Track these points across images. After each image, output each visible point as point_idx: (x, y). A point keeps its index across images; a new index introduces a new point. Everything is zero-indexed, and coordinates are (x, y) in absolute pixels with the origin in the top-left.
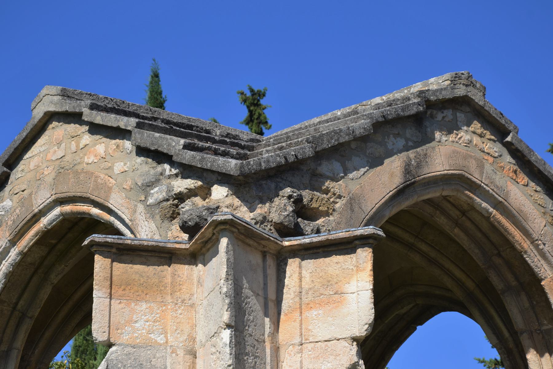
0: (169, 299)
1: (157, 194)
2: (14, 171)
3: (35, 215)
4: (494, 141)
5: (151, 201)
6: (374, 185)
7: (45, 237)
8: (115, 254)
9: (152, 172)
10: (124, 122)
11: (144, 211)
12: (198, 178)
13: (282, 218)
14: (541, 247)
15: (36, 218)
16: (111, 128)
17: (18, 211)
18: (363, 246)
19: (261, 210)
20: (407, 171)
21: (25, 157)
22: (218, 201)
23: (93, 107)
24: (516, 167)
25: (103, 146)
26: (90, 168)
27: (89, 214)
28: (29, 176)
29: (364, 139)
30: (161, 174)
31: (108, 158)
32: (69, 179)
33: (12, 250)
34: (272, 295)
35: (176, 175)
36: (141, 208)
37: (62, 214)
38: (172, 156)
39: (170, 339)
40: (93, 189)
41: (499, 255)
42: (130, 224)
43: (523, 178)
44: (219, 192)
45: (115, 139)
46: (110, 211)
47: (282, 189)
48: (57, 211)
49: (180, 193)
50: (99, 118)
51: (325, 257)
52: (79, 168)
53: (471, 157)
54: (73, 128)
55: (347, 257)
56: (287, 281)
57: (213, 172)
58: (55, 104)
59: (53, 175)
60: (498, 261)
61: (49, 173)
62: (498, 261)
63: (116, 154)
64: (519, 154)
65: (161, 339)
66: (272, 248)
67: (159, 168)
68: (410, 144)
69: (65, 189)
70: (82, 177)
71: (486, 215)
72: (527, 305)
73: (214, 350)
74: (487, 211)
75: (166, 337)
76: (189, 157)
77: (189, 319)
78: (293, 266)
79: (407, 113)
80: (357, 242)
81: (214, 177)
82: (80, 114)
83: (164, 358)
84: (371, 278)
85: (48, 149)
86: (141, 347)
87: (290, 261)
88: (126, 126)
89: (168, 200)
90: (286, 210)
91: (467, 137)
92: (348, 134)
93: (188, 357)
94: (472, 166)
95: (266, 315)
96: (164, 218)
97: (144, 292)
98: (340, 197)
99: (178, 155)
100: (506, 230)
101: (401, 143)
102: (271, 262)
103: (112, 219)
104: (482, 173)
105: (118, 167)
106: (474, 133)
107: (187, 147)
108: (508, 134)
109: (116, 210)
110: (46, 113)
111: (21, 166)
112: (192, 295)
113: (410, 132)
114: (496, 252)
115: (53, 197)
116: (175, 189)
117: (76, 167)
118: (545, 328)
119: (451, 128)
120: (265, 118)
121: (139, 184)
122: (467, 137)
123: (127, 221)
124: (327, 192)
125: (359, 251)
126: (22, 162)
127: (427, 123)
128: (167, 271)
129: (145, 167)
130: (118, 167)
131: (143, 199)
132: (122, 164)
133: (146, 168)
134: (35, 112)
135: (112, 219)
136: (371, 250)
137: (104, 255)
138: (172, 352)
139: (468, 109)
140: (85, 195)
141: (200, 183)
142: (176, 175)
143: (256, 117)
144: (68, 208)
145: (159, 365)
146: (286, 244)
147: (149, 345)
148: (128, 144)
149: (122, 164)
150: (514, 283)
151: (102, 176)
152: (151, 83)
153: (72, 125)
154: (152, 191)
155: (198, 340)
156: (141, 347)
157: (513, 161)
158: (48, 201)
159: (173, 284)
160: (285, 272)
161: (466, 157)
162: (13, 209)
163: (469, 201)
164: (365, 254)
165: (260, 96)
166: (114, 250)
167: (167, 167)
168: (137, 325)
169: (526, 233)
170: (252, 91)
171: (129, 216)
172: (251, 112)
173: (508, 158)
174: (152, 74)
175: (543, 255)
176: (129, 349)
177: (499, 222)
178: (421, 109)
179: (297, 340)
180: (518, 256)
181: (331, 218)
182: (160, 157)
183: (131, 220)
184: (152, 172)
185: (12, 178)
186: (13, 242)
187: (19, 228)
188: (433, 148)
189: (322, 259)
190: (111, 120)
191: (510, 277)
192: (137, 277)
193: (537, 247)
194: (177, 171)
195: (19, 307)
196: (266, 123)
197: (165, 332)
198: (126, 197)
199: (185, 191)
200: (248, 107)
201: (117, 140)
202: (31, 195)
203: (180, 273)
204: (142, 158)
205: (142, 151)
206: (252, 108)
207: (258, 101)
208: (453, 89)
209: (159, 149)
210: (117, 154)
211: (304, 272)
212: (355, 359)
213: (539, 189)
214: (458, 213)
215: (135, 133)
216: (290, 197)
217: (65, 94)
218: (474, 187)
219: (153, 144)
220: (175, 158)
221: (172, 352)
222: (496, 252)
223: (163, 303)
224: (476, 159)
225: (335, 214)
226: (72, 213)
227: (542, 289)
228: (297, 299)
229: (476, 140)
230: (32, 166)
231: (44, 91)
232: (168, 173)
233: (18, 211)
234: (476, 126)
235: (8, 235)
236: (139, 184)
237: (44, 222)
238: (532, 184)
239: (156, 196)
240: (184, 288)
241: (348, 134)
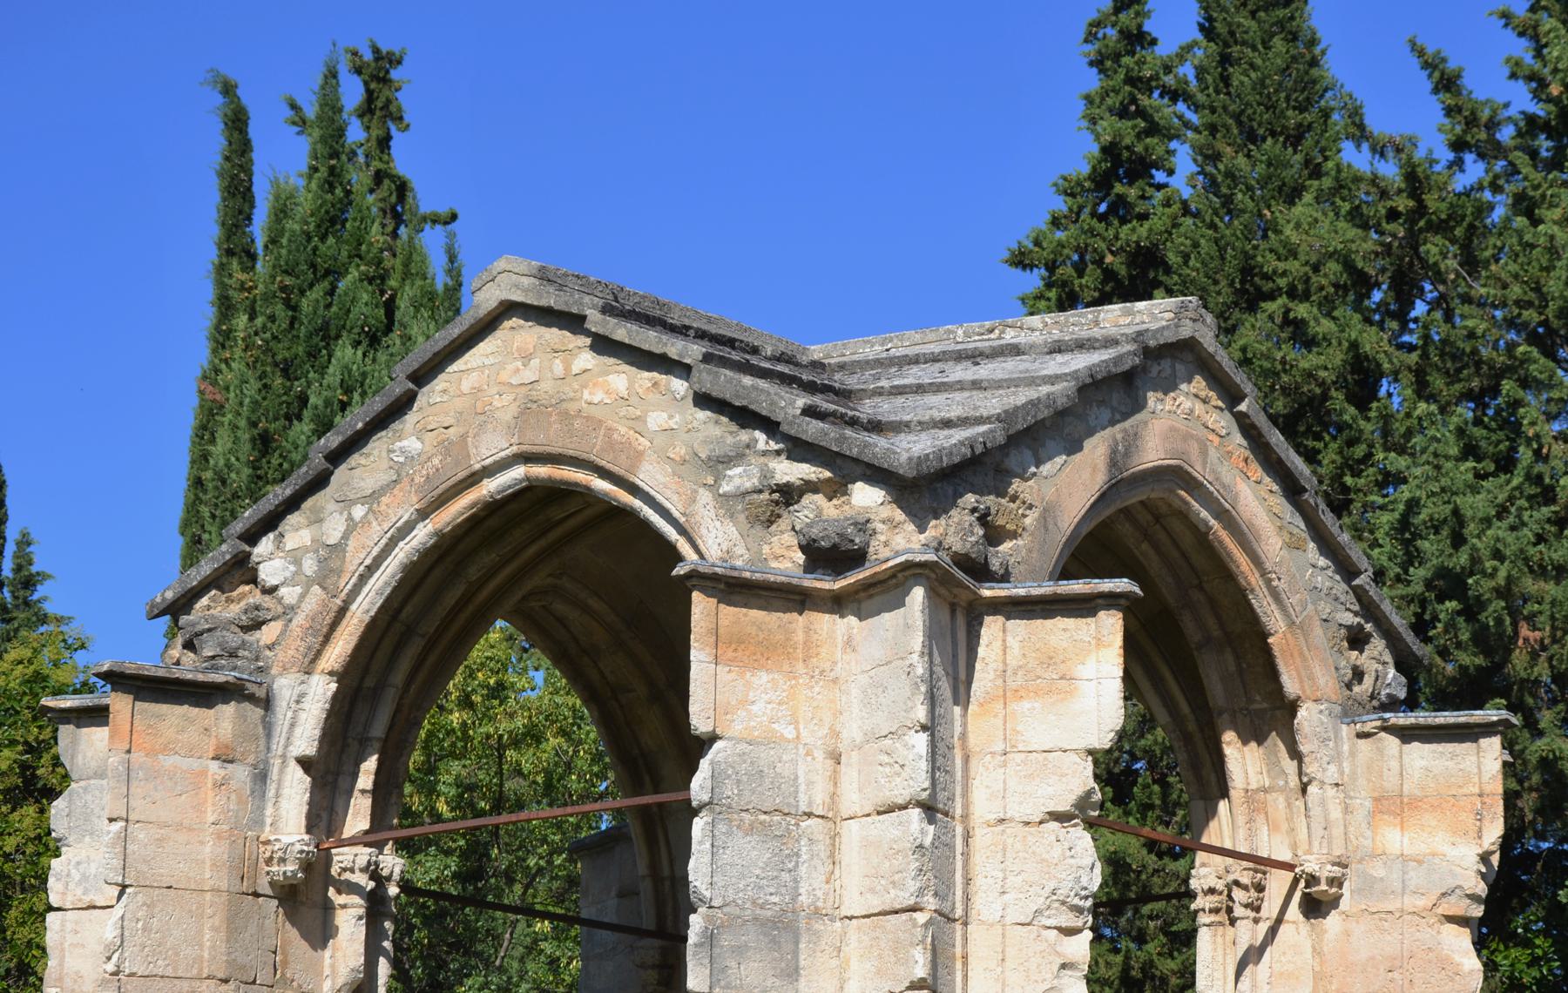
0: (800, 668)
1: (739, 478)
2: (425, 390)
3: (473, 474)
4: (1221, 409)
5: (726, 488)
6: (1066, 487)
7: (493, 509)
8: (722, 591)
9: (730, 440)
10: (674, 347)
11: (712, 503)
12: (825, 464)
13: (968, 546)
14: (1275, 583)
15: (474, 479)
16: (649, 354)
17: (436, 461)
18: (1108, 607)
19: (935, 529)
20: (1114, 462)
21: (450, 369)
22: (867, 509)
23: (607, 310)
24: (1248, 453)
25: (621, 378)
26: (597, 413)
27: (588, 488)
28: (459, 404)
29: (1062, 414)
30: (748, 446)
31: (634, 400)
32: (550, 423)
33: (421, 525)
34: (963, 676)
35: (778, 453)
36: (705, 496)
37: (528, 478)
38: (778, 424)
39: (804, 733)
40: (603, 449)
41: (1201, 588)
42: (682, 520)
43: (1256, 471)
44: (866, 496)
45: (649, 370)
46: (634, 490)
47: (961, 496)
48: (518, 472)
49: (788, 485)
50: (622, 332)
51: (1045, 618)
52: (572, 407)
53: (1192, 436)
54: (554, 335)
55: (1081, 622)
56: (981, 651)
57: (856, 460)
58: (526, 291)
59: (513, 410)
60: (1196, 596)
61: (505, 407)
62: (1196, 596)
63: (651, 396)
64: (1254, 432)
65: (789, 733)
66: (964, 597)
67: (744, 436)
68: (1118, 417)
69: (541, 438)
70: (577, 424)
71: (1203, 529)
72: (1232, 668)
73: (886, 759)
74: (1206, 523)
75: (797, 729)
76: (813, 429)
77: (832, 701)
78: (992, 628)
79: (1120, 370)
80: (1100, 601)
81: (859, 470)
82: (584, 318)
83: (794, 762)
84: (1121, 660)
85: (502, 365)
86: (758, 744)
87: (988, 619)
88: (680, 355)
89: (760, 491)
90: (973, 534)
91: (1187, 404)
92: (1048, 407)
93: (830, 762)
94: (1194, 450)
95: (956, 703)
96: (754, 520)
97: (766, 653)
98: (1030, 507)
99: (791, 423)
100: (1229, 554)
101: (1106, 414)
102: (961, 621)
103: (637, 503)
104: (1205, 463)
105: (657, 420)
106: (1196, 396)
107: (810, 412)
108: (1241, 399)
109: (652, 493)
110: (502, 303)
111: (440, 383)
112: (835, 663)
113: (1117, 397)
114: (1196, 582)
115: (514, 449)
116: (778, 476)
117: (564, 405)
118: (1256, 706)
119: (1169, 386)
120: (400, 109)
121: (703, 456)
122: (1187, 404)
123: (676, 514)
124: (1014, 499)
125: (1102, 614)
126: (442, 377)
127: (1138, 383)
128: (799, 623)
129: (711, 429)
130: (657, 420)
131: (710, 481)
132: (665, 415)
133: (716, 431)
134: (480, 297)
135: (637, 503)
136: (1121, 615)
137: (703, 590)
138: (807, 754)
139: (1190, 357)
140: (584, 456)
141: (828, 474)
142: (778, 453)
143: (379, 104)
144: (542, 471)
145: (786, 773)
146: (986, 593)
147: (772, 740)
148: (679, 386)
149: (665, 415)
150: (1216, 633)
151: (623, 430)
152: (323, 88)
153: (555, 330)
154: (729, 473)
155: (844, 735)
156: (758, 744)
157: (1245, 443)
158: (503, 454)
159: (807, 643)
160: (978, 637)
161: (1187, 437)
162: (424, 457)
163: (1184, 508)
164: (1111, 620)
165: (391, 62)
166: (722, 586)
167: (760, 436)
168: (754, 708)
169: (1257, 561)
170: (376, 50)
171: (680, 507)
172: (370, 93)
173: (1238, 439)
174: (324, 70)
175: (1275, 595)
176: (743, 747)
177: (1221, 542)
178: (1137, 361)
179: (999, 747)
180: (1240, 597)
181: (1020, 542)
182: (745, 417)
183: (684, 514)
184: (730, 440)
185: (421, 401)
186: (423, 514)
187: (439, 491)
188: (1146, 423)
189: (1039, 621)
190: (650, 339)
191: (1211, 623)
192: (753, 631)
193: (1268, 582)
194: (781, 446)
195: (403, 615)
196: (401, 118)
197: (795, 722)
198: (674, 474)
199: (798, 483)
200: (366, 83)
201: (655, 374)
202: (464, 437)
203: (816, 626)
204: (708, 413)
205: (703, 400)
206: (373, 86)
207: (387, 72)
208: (1177, 326)
209: (752, 407)
210: (653, 397)
211: (1009, 639)
212: (1092, 783)
213: (1275, 488)
214: (1150, 518)
215: (700, 372)
216: (974, 510)
217: (544, 276)
218: (1193, 485)
219: (738, 396)
220: (784, 428)
221: (807, 754)
222: (1196, 582)
223: (792, 675)
224: (1199, 440)
225: (1025, 535)
226: (550, 479)
227: (1267, 651)
228: (999, 682)
229: (1199, 408)
230: (466, 386)
231: (501, 264)
232: (761, 445)
233: (436, 461)
234: (1199, 384)
235: (415, 499)
236: (703, 456)
237: (490, 487)
238: (1267, 480)
239: (737, 481)
240: (823, 651)
241: (1048, 407)
